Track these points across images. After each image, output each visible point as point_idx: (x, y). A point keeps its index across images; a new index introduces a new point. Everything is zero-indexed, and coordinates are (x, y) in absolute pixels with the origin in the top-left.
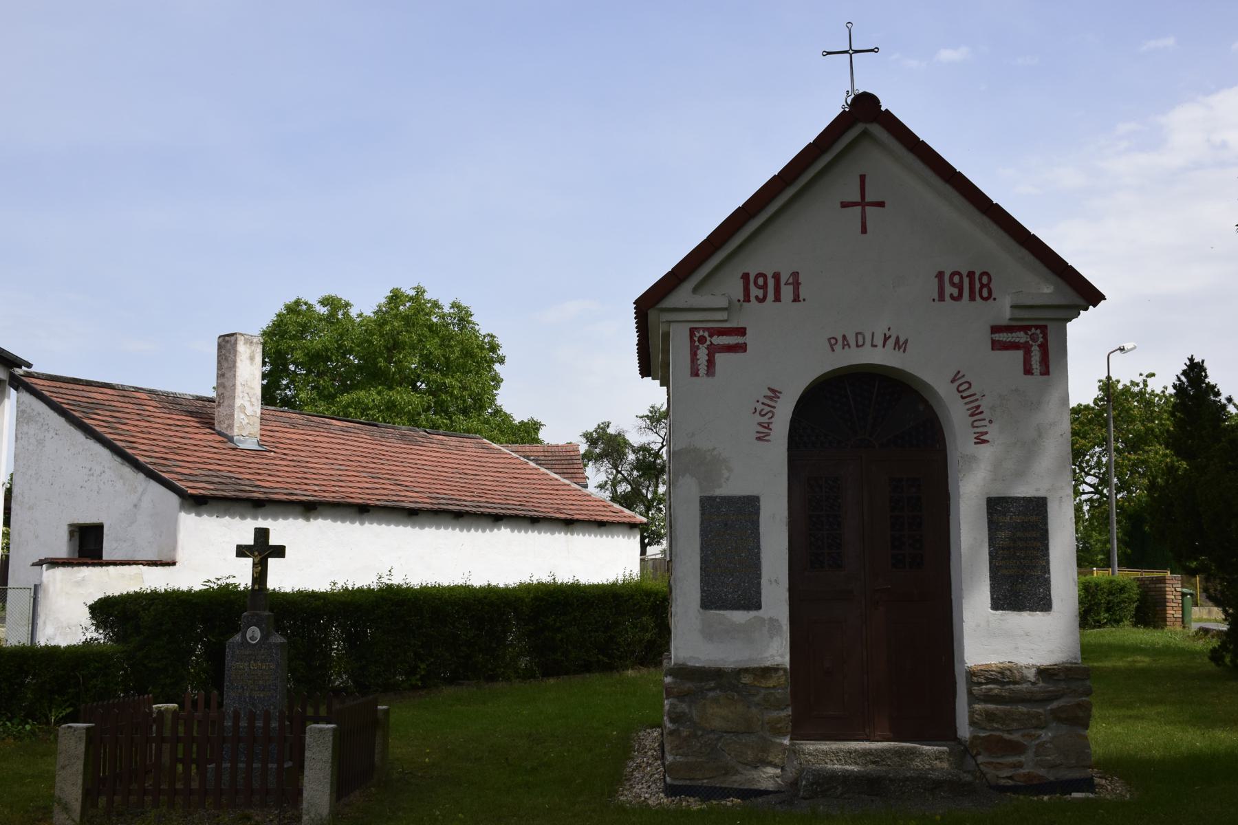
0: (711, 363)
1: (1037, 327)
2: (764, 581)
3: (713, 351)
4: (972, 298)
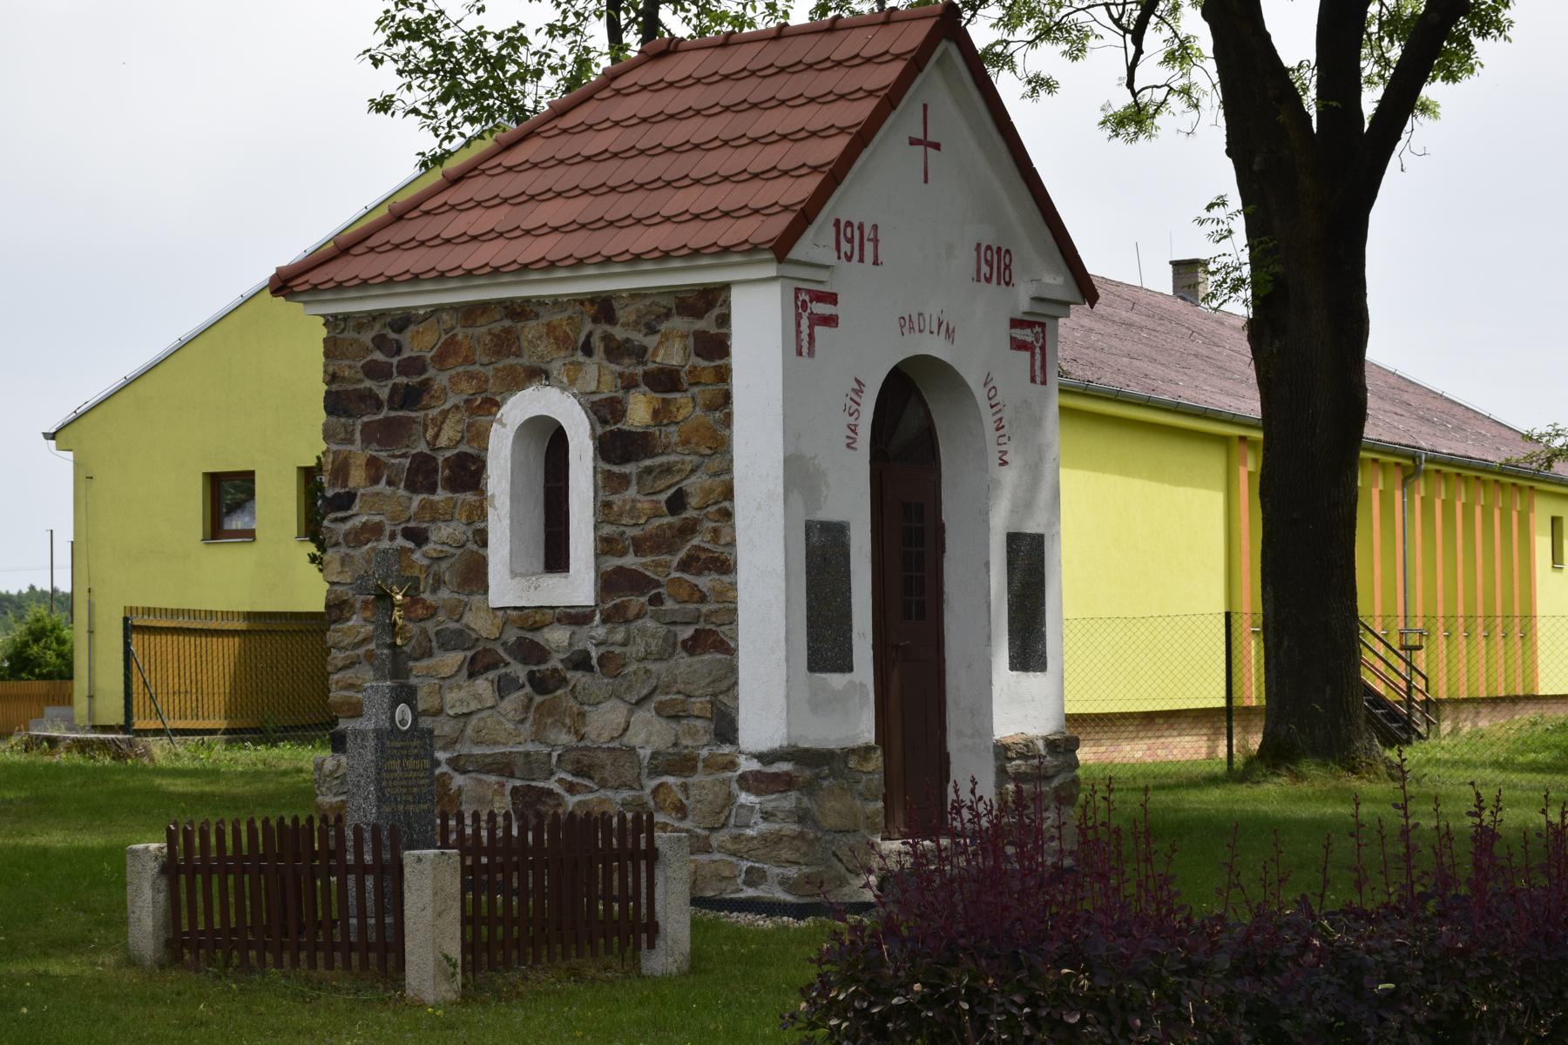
2: (854, 635)
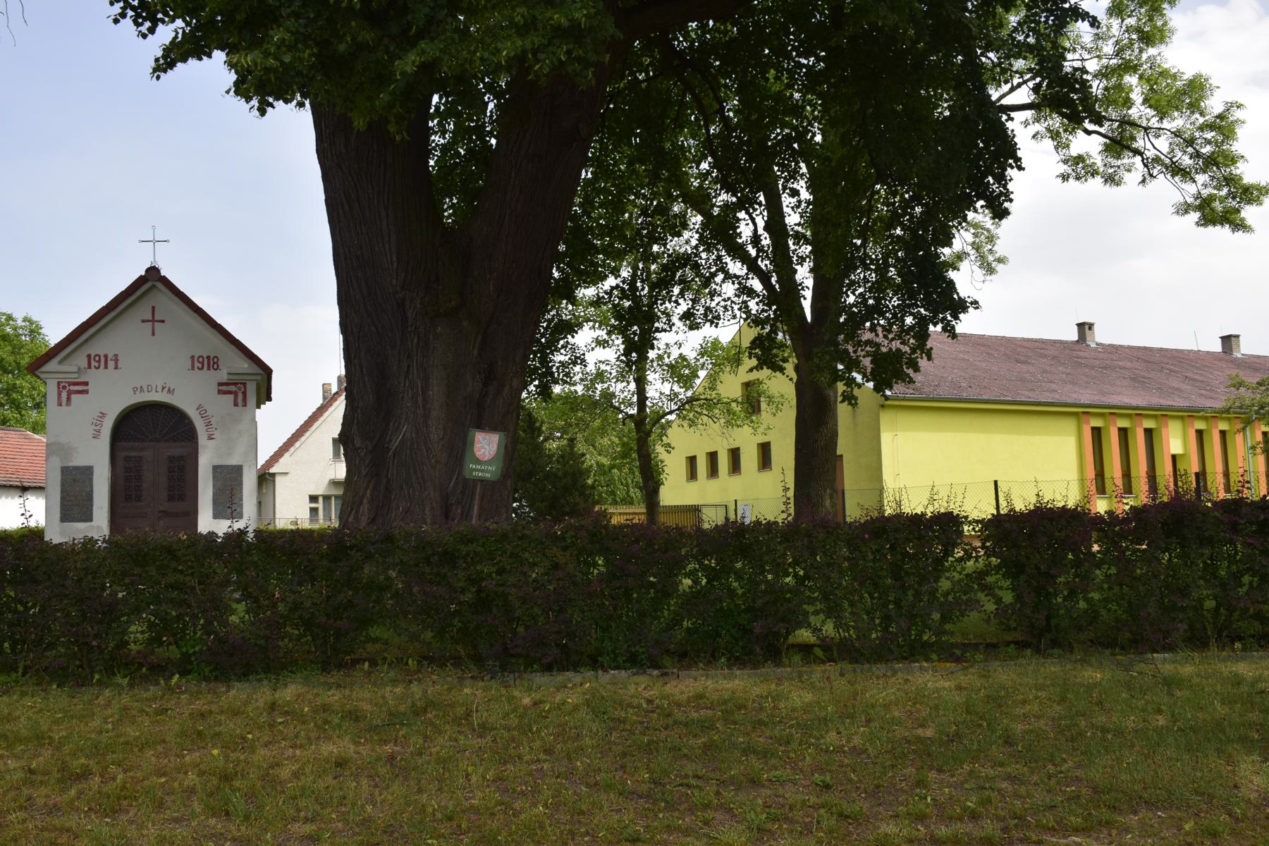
0: (69, 399)
1: (241, 383)
2: (94, 508)
3: (70, 393)
4: (209, 369)
